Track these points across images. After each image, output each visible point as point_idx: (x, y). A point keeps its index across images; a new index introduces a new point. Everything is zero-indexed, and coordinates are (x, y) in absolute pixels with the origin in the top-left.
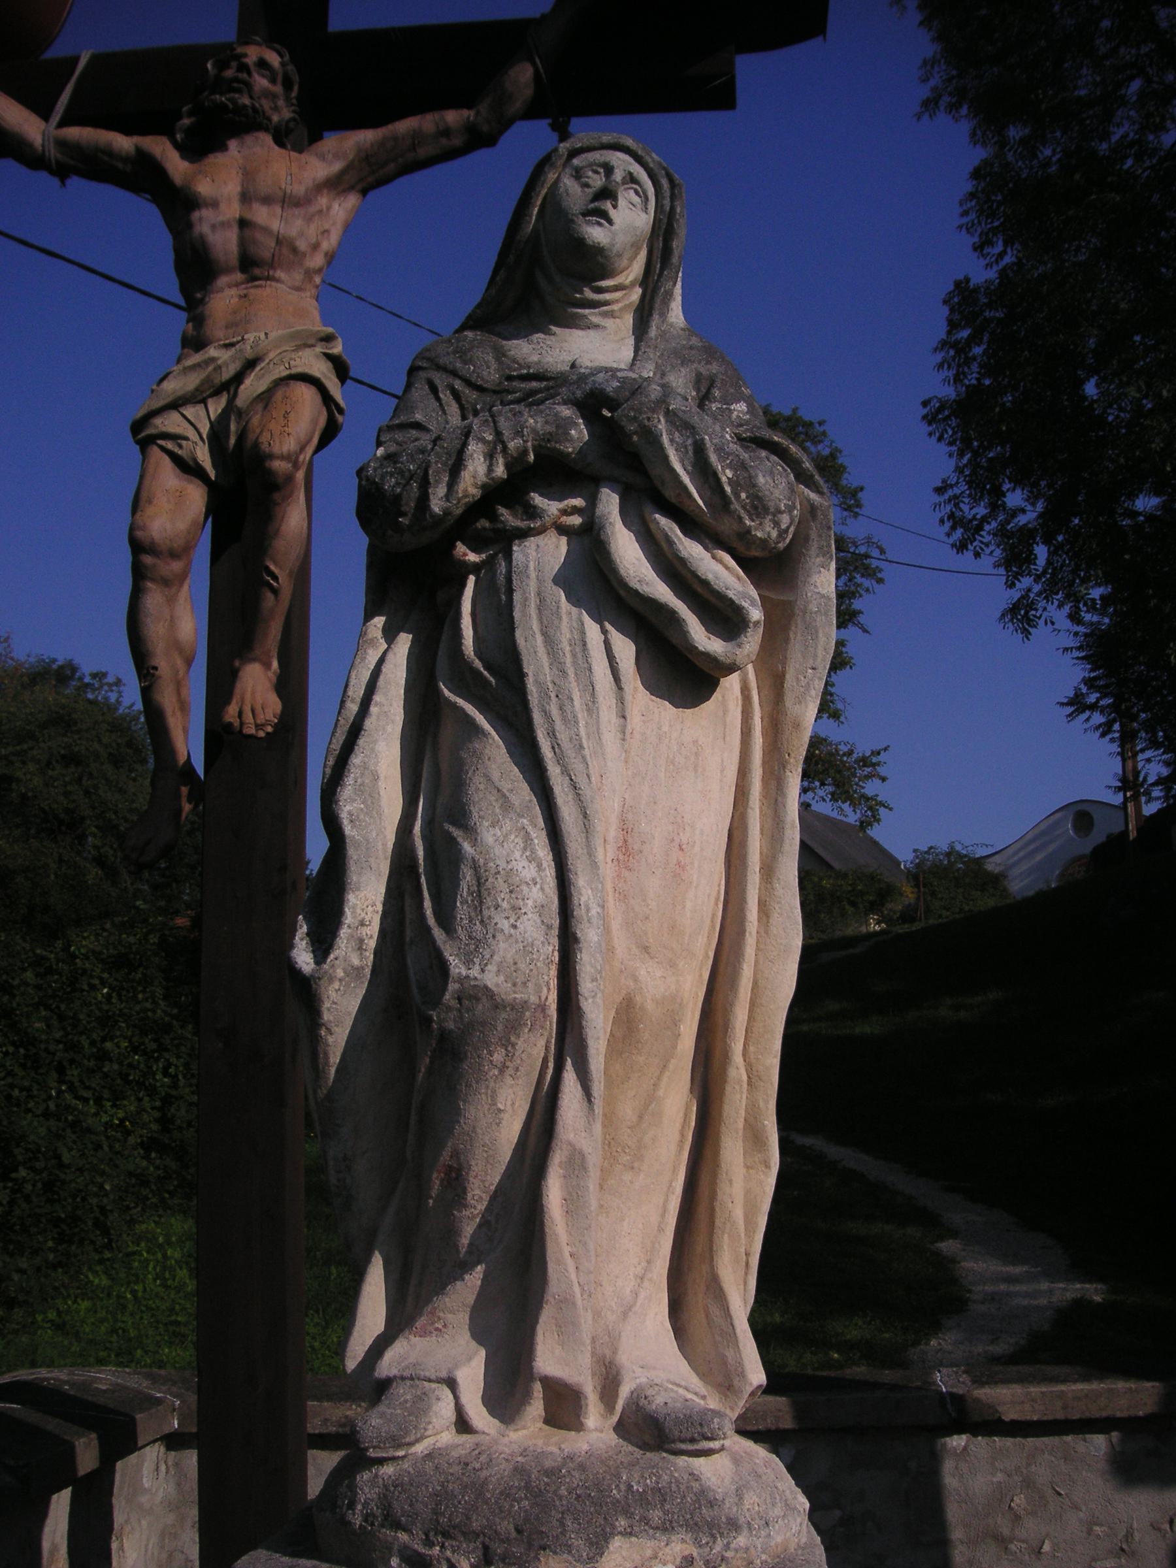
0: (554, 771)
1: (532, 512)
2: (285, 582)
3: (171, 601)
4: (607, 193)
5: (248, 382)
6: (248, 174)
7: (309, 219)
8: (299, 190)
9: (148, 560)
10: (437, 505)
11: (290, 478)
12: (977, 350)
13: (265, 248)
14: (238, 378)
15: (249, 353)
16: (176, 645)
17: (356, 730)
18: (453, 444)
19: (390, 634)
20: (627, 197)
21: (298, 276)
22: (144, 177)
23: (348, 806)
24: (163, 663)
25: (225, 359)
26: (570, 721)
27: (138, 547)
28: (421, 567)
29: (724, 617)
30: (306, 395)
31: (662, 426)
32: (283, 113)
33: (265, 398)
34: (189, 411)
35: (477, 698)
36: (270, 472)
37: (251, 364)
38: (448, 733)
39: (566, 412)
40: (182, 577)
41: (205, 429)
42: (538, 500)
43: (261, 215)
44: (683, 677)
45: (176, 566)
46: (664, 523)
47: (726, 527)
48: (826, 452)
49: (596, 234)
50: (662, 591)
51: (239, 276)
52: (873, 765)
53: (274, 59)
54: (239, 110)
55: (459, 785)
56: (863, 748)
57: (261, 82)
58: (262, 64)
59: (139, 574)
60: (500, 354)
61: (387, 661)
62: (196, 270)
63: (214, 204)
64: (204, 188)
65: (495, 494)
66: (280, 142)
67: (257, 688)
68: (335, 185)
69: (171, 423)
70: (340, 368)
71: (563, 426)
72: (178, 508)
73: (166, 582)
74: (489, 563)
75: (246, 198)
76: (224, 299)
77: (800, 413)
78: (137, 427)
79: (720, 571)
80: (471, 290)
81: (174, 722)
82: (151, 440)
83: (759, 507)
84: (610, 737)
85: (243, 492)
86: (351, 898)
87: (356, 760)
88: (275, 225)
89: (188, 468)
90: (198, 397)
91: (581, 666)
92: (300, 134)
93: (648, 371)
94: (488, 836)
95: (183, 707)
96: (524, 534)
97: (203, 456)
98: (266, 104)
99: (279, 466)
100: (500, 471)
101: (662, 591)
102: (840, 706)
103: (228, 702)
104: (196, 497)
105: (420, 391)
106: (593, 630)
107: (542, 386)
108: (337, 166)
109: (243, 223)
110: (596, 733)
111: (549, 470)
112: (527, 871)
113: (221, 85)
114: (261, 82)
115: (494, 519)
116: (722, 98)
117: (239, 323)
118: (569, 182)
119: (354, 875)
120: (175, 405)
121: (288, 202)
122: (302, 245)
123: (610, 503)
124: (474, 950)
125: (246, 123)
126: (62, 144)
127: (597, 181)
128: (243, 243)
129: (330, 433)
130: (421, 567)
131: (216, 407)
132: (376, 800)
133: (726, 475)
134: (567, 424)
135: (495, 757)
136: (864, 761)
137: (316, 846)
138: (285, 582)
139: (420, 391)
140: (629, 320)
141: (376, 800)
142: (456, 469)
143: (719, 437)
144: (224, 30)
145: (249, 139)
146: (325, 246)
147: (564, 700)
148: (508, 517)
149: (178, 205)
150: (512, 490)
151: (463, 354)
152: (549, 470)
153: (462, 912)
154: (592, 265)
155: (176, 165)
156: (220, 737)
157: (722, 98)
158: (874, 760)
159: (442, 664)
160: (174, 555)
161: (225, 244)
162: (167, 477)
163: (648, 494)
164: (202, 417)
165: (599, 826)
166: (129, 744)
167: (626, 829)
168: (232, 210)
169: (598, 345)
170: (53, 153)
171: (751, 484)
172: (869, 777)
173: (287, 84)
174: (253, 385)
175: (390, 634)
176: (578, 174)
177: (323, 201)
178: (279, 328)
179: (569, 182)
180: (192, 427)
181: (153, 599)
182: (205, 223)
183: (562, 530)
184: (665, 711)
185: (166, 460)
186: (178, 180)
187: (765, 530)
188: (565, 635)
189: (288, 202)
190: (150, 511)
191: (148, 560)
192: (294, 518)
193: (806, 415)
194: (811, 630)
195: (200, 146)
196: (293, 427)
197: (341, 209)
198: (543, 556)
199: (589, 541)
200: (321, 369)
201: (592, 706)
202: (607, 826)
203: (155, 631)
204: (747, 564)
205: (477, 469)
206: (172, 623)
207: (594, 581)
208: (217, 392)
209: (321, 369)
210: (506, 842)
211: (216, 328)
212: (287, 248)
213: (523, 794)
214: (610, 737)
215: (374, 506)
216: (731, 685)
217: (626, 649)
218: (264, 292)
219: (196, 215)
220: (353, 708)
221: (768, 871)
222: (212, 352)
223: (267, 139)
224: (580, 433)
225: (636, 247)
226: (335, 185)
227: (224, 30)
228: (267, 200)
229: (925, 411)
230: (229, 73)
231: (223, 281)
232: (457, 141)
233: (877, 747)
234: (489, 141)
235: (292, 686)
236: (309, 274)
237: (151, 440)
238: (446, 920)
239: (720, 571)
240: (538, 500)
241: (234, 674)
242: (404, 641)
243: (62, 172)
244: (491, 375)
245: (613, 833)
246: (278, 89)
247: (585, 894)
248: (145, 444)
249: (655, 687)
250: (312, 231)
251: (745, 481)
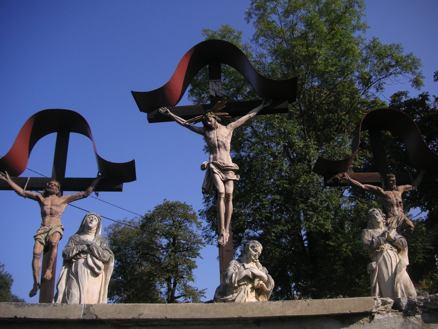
0: (80, 284)
1: (81, 256)
2: (53, 259)
3: (38, 261)
4: (92, 221)
5: (50, 232)
6: (52, 201)
7: (60, 208)
8: (59, 204)
9: (35, 256)
10: (70, 256)
11: (55, 246)
12: (211, 199)
13: (54, 212)
14: (49, 231)
15: (50, 227)
16: (38, 267)
17: (61, 279)
18: (72, 249)
19: (65, 268)
20: (94, 221)
21: (58, 216)
22: (37, 199)
23: (59, 287)
24: (36, 269)
25: (47, 228)
26: (82, 279)
27: (34, 254)
28: (68, 262)
29: (99, 268)
30: (58, 234)
31: (94, 248)
32: (58, 191)
33: (53, 234)
34: (42, 235)
35: (73, 276)
36: (52, 245)
37: (51, 229)
38: (70, 279)
39: (85, 246)
40: (40, 258)
41: (44, 238)
42: (81, 255)
43: (54, 208)
44: (96, 275)
45: (39, 256)
46: (94, 258)
47: (100, 258)
48: (193, 213)
49: (90, 225)
50: (93, 265)
51: (50, 216)
52: (204, 293)
53: (57, 184)
54: (51, 192)
55: (71, 285)
56: (200, 289)
57: (55, 187)
58: (55, 185)
59: (34, 257)
60: (79, 237)
61: (64, 271)
62: (44, 214)
63: (47, 206)
64: (46, 203)
65: (76, 255)
66: (57, 196)
67: (49, 273)
68: (64, 203)
69: (39, 237)
70: (63, 229)
71: (84, 247)
72: (40, 249)
73: (38, 259)
74: (76, 261)
75: (51, 205)
76: (48, 219)
77: (186, 203)
78: (35, 237)
79: (100, 263)
80: (77, 230)
81: (37, 277)
82: (36, 239)
83: (104, 257)
84: (87, 280)
85: (48, 247)
86: (59, 296)
87: (60, 282)
88: (55, 209)
89: (42, 243)
90: (43, 233)
91: (84, 273)
92: (60, 195)
93: (95, 241)
94: (73, 290)
95: (39, 275)
96: (80, 258)
97: (44, 242)
98: (55, 191)
99: (54, 244)
100: (77, 252)
101: (93, 265)
102: (194, 278)
103: (45, 275)
104: (42, 247)
105: (70, 242)
106: (86, 269)
107: (82, 242)
108: (65, 200)
109: (51, 209)
110: (85, 280)
111: (83, 252)
112: (76, 293)
113: (49, 188)
114: (55, 187)
115: (77, 257)
116: (120, 190)
117: (49, 223)
118: (88, 218)
119: (59, 294)
120: (40, 234)
121: (57, 206)
122: (59, 212)
123: (89, 255)
124: (71, 301)
125: (52, 193)
126: (26, 193)
127: (91, 219)
128: (51, 211)
129: (61, 238)
130: (68, 262)
131: (46, 235)
132: (62, 286)
133: (101, 253)
134: (84, 247)
135: (75, 281)
136: (200, 292)
137: (55, 291)
138: (53, 259)
139: (70, 242)
140: (94, 234)
141: (62, 286)
142: (73, 252)
143: (100, 249)
144: (50, 175)
145: (52, 195)
146: (62, 212)
147: (82, 277)
148: (78, 257)
149: (42, 205)
150: (79, 254)
151: (75, 237)
152: (83, 252)
153: (70, 297)
154: (90, 228)
155: (42, 198)
156: (43, 280)
157: (120, 190)
158: (204, 292)
159: (70, 272)
160: (39, 255)
161: (48, 211)
162: (39, 244)
163: (93, 255)
164: (44, 236)
165: (84, 289)
166: (5, 283)
167: (88, 290)
168: (49, 206)
169: (90, 238)
170: (24, 195)
171: (103, 254)
172: (202, 296)
173: (58, 187)
174: (51, 233)
175: (65, 268)
176: (89, 218)
177: (62, 205)
178: (55, 224)
179: (88, 218)
180: (42, 237)
181: (36, 261)
182: (46, 208)
183: (84, 258)
184: (93, 278)
185: (39, 242)
186: (42, 201)
187: (105, 259)
188: (83, 269)
189: (57, 206)
190: (36, 249)
191: (35, 256)
192: (55, 251)
193: (188, 204)
194: (110, 269)
195: (46, 195)
196: (55, 239)
197: (65, 206)
198: (81, 261)
199: (86, 259)
200: (60, 230)
201: (85, 277)
202: (86, 289)
203: (36, 265)
204: (103, 263)
205: (75, 252)
206: (38, 264)
207: (86, 264)
208: (46, 233)
209: (60, 230)
210: (75, 291)
211: (46, 223)
212: (57, 212)
213: (77, 286)
214: (87, 280)
215: (64, 255)
216: (101, 275)
217: (89, 271)
218: (53, 218)
219: (44, 207)
220: (60, 276)
221: (104, 295)
222: (46, 227)
223: (55, 195)
224: (86, 248)
225: (95, 226)
226: (64, 203)
227: (50, 175)
228: (54, 205)
229: (199, 213)
230: (50, 186)
231: (47, 216)
232: (82, 197)
233: (205, 288)
234: (86, 197)
235: (53, 273)
236: (59, 216)
237: (36, 239)
238: (68, 298)
239: (100, 263)
240: (81, 255)
241: (46, 271)
242: (67, 269)
243: (25, 197)
244: (78, 240)
245: (86, 290)
246: (57, 188)
247: (82, 296)
248: (36, 239)
249: (92, 275)
250: (60, 210)
251: (103, 254)
